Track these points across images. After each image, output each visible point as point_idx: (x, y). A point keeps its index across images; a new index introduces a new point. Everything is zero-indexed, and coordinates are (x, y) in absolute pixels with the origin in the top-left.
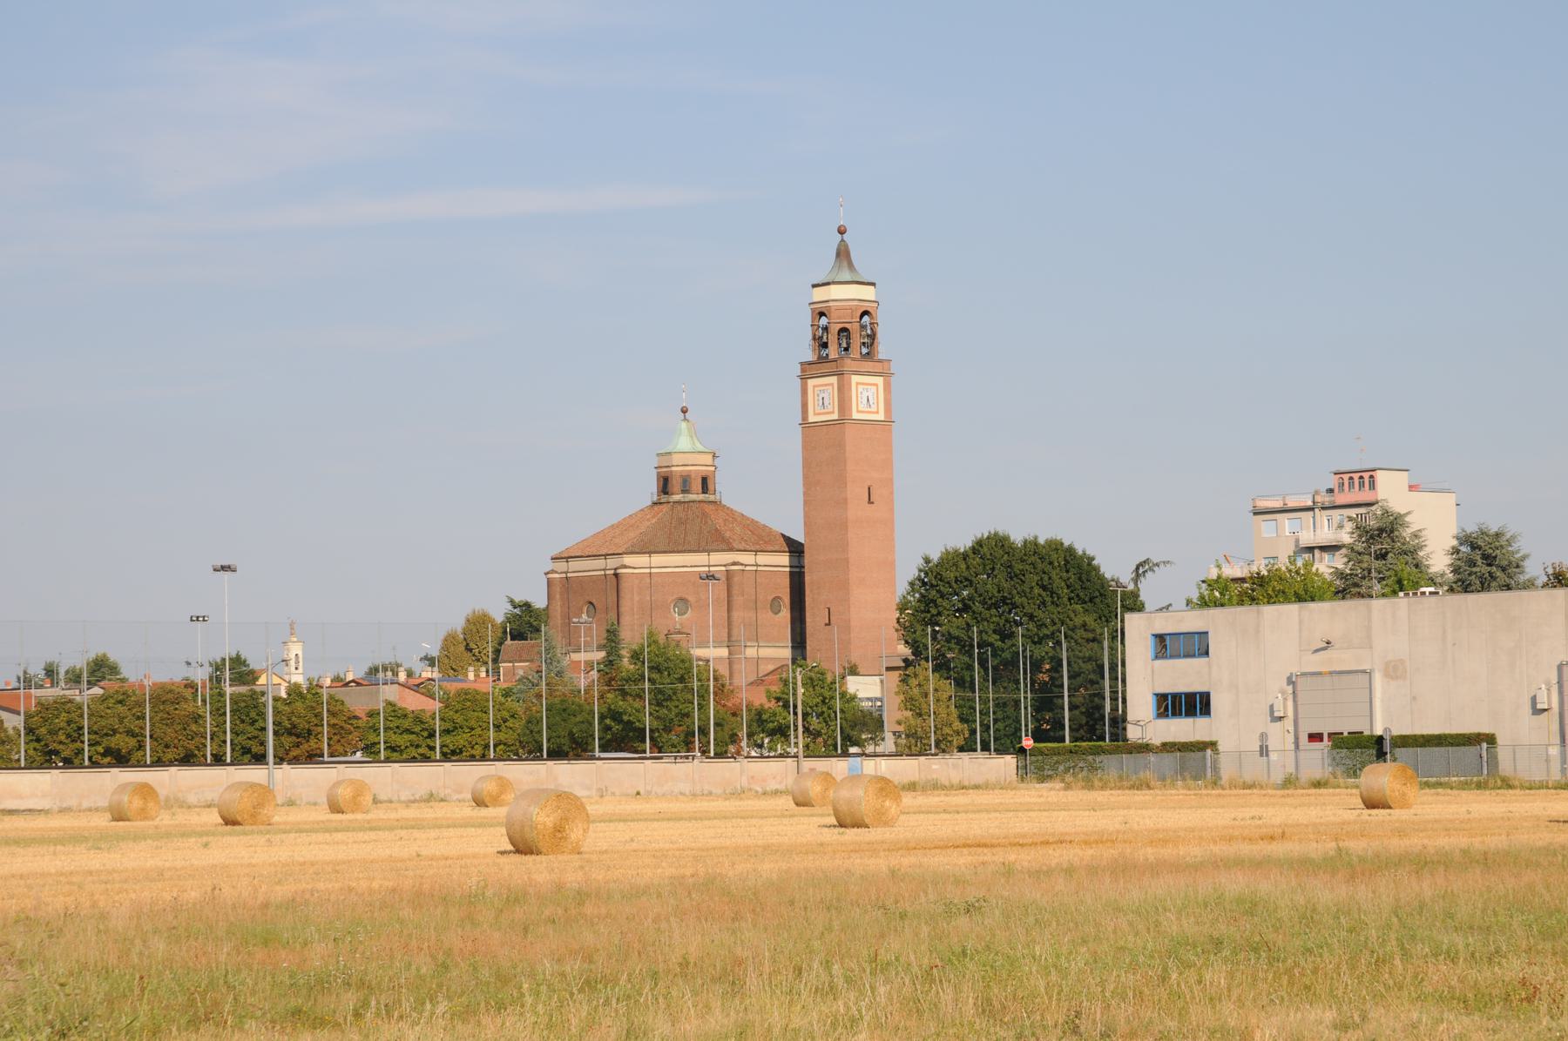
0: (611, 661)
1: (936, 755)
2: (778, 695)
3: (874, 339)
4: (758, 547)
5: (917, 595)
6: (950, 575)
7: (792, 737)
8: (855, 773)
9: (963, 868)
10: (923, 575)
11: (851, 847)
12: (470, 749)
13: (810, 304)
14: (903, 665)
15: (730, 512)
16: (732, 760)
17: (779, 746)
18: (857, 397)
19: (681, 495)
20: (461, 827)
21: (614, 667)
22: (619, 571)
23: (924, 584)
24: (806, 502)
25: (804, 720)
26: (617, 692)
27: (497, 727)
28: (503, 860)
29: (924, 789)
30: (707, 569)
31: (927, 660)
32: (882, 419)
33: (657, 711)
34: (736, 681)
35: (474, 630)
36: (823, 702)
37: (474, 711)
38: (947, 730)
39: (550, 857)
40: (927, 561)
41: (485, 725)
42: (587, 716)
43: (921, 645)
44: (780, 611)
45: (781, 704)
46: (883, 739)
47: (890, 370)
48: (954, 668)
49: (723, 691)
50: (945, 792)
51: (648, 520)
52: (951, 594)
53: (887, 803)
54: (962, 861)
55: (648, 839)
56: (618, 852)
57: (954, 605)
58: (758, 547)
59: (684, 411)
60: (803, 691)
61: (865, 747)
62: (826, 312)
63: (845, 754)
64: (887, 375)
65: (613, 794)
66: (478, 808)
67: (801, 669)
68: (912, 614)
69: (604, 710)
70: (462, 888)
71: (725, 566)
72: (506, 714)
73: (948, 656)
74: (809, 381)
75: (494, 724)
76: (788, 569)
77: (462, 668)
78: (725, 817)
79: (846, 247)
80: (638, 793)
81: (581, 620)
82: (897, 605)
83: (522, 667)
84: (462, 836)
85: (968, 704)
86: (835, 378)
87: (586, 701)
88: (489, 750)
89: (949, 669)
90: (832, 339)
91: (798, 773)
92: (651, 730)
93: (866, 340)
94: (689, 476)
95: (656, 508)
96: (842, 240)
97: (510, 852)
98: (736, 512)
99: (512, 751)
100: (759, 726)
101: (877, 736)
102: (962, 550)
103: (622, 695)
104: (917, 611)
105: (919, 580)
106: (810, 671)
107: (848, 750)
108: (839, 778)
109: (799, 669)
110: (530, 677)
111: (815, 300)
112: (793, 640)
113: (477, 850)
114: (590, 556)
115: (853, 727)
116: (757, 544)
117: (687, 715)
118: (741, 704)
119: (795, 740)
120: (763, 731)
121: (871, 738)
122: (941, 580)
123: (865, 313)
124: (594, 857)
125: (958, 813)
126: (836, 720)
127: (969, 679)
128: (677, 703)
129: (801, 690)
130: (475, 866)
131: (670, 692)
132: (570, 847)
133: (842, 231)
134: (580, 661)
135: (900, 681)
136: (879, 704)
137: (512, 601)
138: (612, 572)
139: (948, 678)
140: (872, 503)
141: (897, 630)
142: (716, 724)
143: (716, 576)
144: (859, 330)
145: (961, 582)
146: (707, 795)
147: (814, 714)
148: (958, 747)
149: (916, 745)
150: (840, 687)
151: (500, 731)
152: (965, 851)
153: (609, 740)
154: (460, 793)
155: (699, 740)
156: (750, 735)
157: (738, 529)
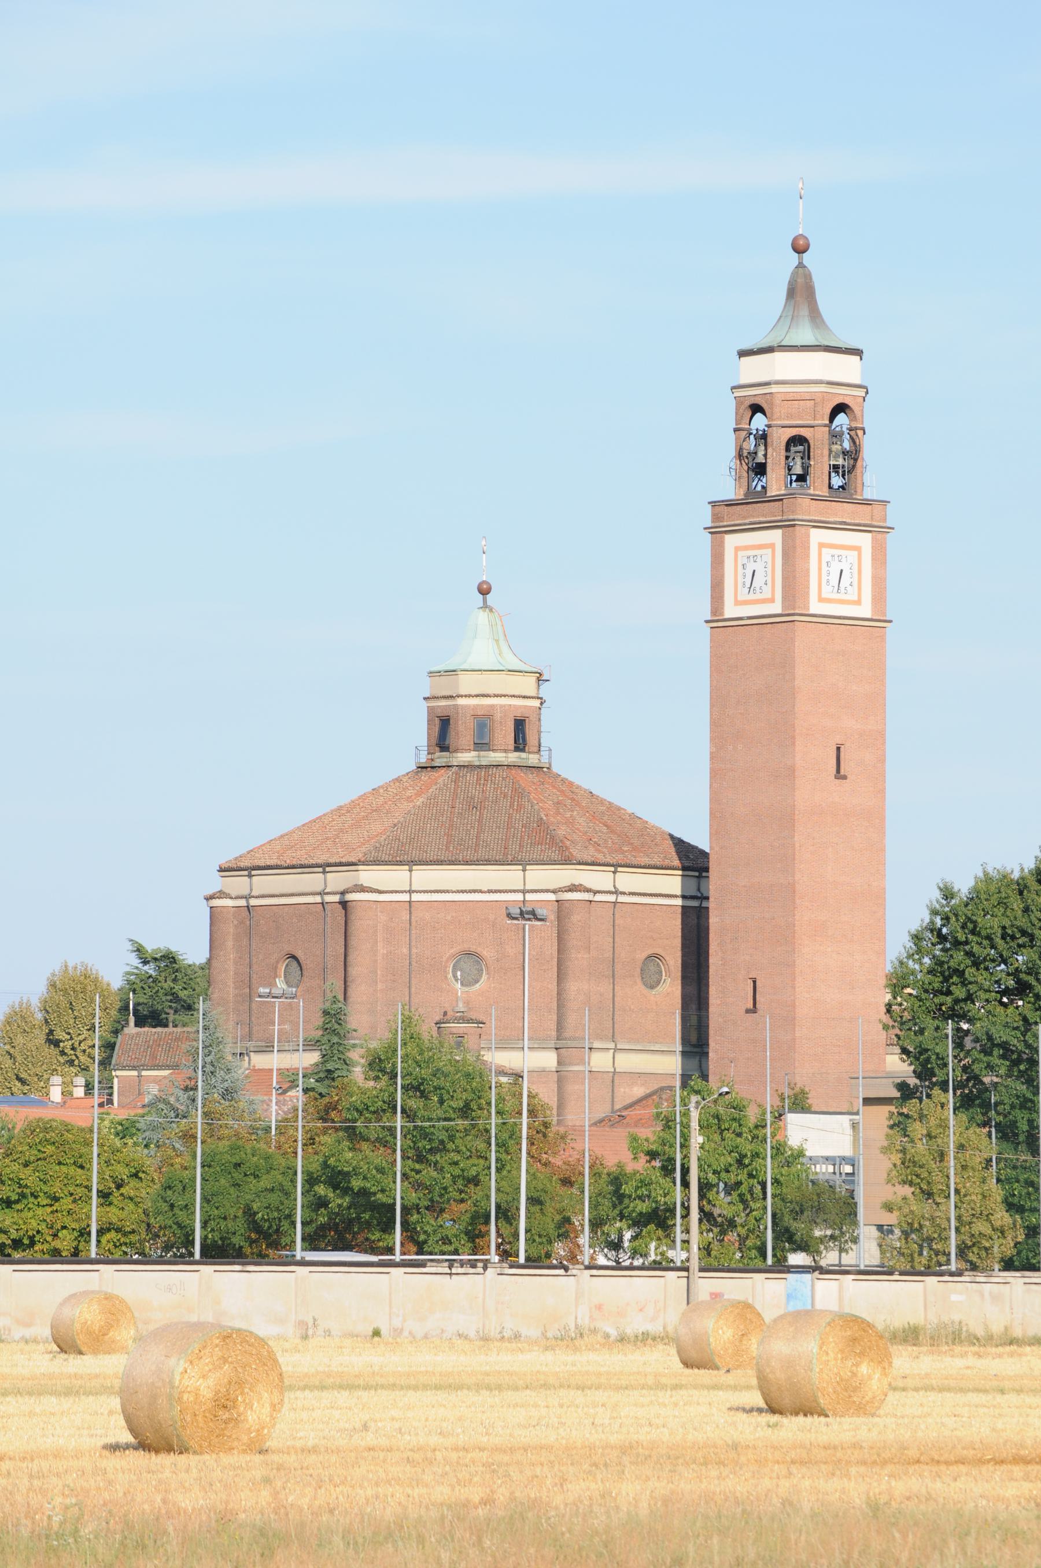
0: (329, 1071)
1: (959, 1273)
2: (654, 1147)
3: (856, 460)
4: (621, 856)
5: (927, 960)
6: (991, 924)
7: (678, 1229)
8: (800, 1306)
9: (1014, 1506)
10: (938, 922)
11: (793, 1454)
12: (50, 1239)
13: (733, 388)
14: (898, 1095)
15: (568, 788)
16: (562, 1272)
17: (653, 1245)
18: (820, 569)
19: (474, 754)
20: (30, 1394)
21: (335, 1084)
22: (350, 897)
23: (942, 938)
24: (714, 774)
25: (702, 1196)
26: (341, 1134)
27: (104, 1196)
28: (114, 1462)
29: (935, 1340)
30: (519, 897)
31: (944, 1086)
32: (868, 615)
33: (418, 1172)
34: (571, 1118)
35: (64, 1004)
36: (740, 1162)
37: (60, 1163)
38: (981, 1227)
39: (206, 1457)
40: (948, 893)
41: (80, 1191)
42: (280, 1177)
43: (934, 1057)
44: (658, 982)
45: (657, 1164)
46: (855, 1240)
47: (885, 520)
48: (997, 1104)
49: (545, 1136)
50: (975, 1349)
51: (409, 799)
52: (993, 961)
53: (864, 1369)
54: (1011, 1491)
55: (397, 1425)
56: (338, 1451)
57: (998, 982)
58: (618, 858)
59: (484, 590)
60: (700, 1139)
61: (819, 1253)
62: (765, 406)
63: (781, 1267)
64: (878, 529)
65: (328, 1333)
66: (63, 1356)
67: (699, 1098)
68: (918, 998)
69: (315, 1167)
70: (33, 1519)
71: (554, 892)
72: (123, 1172)
73: (987, 1080)
74: (728, 538)
75: (98, 1191)
76: (679, 902)
77: (40, 1078)
78: (544, 1385)
79: (808, 277)
80: (376, 1333)
81: (275, 991)
82: (889, 977)
83: (156, 1080)
84: (31, 1414)
85: (1023, 1177)
86: (778, 533)
87: (279, 1148)
88: (88, 1242)
89: (986, 1106)
90: (775, 458)
91: (688, 1303)
92: (404, 1208)
93: (840, 462)
94: (490, 717)
95: (425, 776)
96: (801, 265)
97: (127, 1447)
98: (578, 787)
99: (131, 1244)
100: (614, 1206)
101: (843, 1234)
102: (1016, 875)
103: (351, 1140)
104: (926, 991)
105: (932, 931)
106: (715, 1101)
107: (785, 1259)
108: (768, 1316)
109: (694, 1098)
110: (172, 1100)
111: (743, 381)
112: (685, 1040)
113: (61, 1441)
114: (293, 867)
115: (798, 1213)
116: (620, 851)
117: (475, 1181)
118: (580, 1161)
119: (685, 1237)
120: (622, 1216)
121: (832, 1237)
122: (973, 932)
123: (840, 408)
124: (291, 1460)
125: (1002, 1392)
126: (765, 1198)
127: (1025, 1128)
128: (456, 1157)
129: (697, 1139)
130: (58, 1475)
131: (443, 1136)
132: (245, 1438)
133: (800, 248)
134: (271, 1070)
135: (891, 1127)
136: (848, 1169)
137: (139, 950)
138: (336, 898)
139: (985, 1124)
140: (845, 777)
141: (886, 1027)
142: (532, 1201)
143: (540, 912)
144: (826, 442)
145: (1013, 938)
146: (510, 1340)
147: (722, 1185)
148: (1002, 1260)
149: (921, 1254)
150: (773, 1136)
151: (110, 1204)
152: (1018, 1470)
153: (322, 1227)
154: (28, 1325)
155: (498, 1232)
156: (596, 1224)
157: (581, 821)
